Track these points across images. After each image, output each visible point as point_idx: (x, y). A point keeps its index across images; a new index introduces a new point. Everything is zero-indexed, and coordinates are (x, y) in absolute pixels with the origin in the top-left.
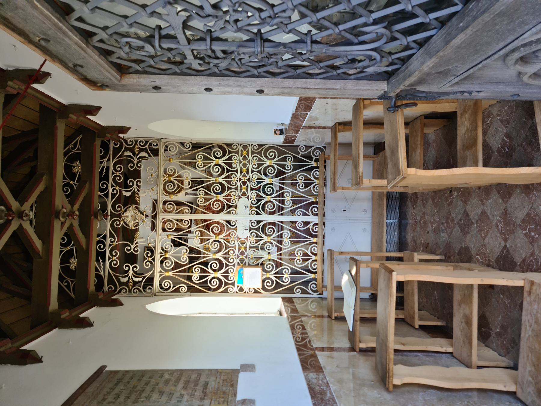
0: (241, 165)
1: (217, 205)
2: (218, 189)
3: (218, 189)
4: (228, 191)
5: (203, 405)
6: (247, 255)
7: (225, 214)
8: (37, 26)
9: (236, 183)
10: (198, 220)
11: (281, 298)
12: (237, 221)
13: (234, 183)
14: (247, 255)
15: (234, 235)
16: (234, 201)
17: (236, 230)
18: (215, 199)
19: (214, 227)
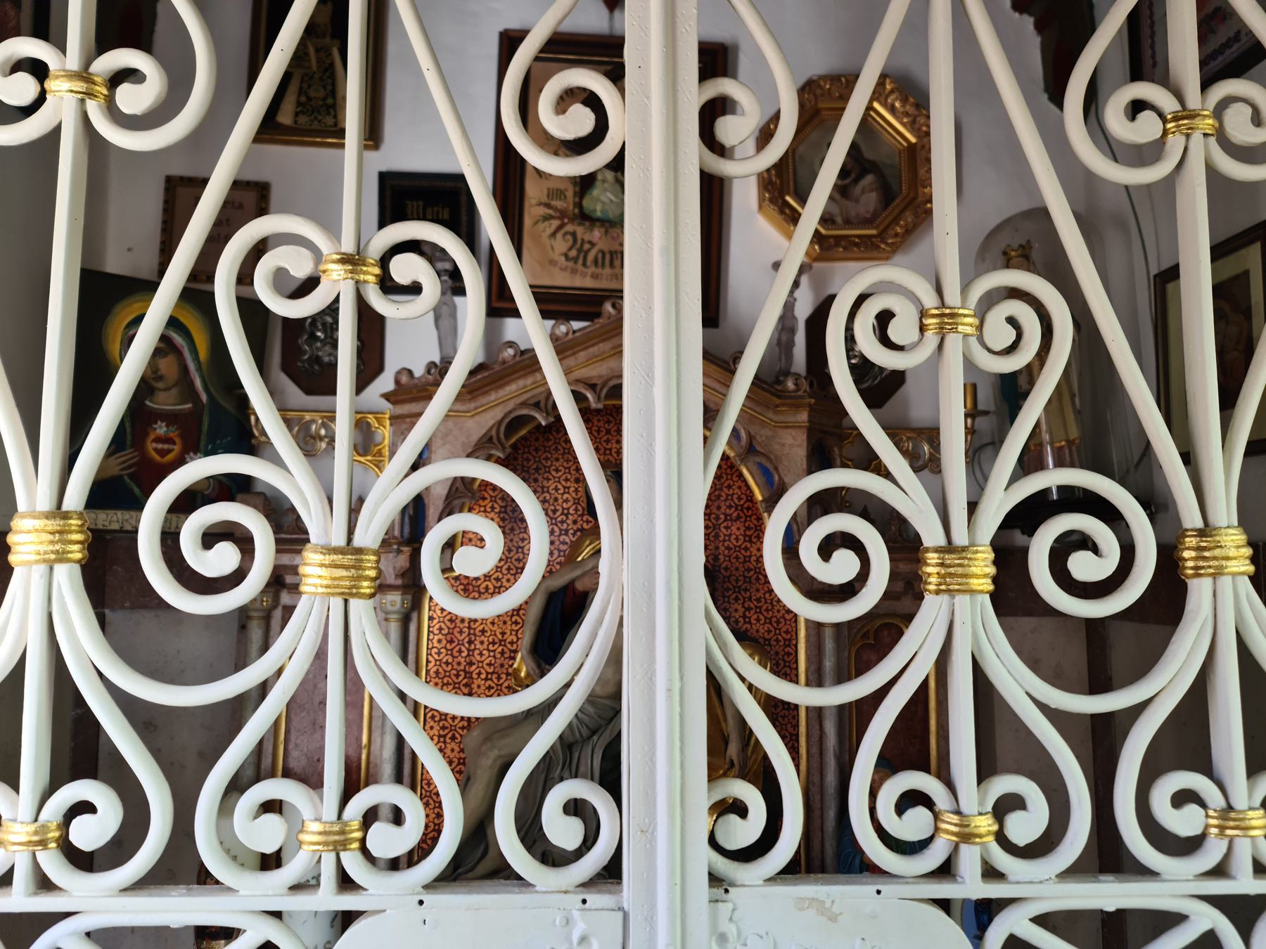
0: (1209, 919)
1: (843, 567)
2: (1083, 566)
3: (1083, 566)
4: (1055, 716)
5: (205, 934)
6: (1219, 902)
7: (715, 688)
8: (647, 820)
9: (1190, 846)
10: (618, 352)
11: (1247, 578)
12: (612, 872)
13: (1183, 822)
14: (1219, 902)
15: (387, 840)
16: (914, 825)
17: (455, 874)
18: (931, 534)
19: (511, 519)
